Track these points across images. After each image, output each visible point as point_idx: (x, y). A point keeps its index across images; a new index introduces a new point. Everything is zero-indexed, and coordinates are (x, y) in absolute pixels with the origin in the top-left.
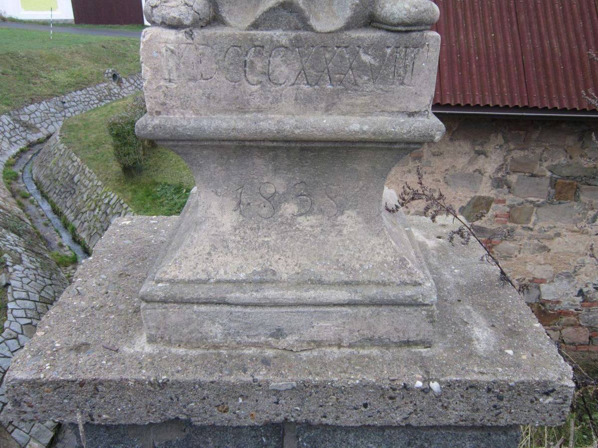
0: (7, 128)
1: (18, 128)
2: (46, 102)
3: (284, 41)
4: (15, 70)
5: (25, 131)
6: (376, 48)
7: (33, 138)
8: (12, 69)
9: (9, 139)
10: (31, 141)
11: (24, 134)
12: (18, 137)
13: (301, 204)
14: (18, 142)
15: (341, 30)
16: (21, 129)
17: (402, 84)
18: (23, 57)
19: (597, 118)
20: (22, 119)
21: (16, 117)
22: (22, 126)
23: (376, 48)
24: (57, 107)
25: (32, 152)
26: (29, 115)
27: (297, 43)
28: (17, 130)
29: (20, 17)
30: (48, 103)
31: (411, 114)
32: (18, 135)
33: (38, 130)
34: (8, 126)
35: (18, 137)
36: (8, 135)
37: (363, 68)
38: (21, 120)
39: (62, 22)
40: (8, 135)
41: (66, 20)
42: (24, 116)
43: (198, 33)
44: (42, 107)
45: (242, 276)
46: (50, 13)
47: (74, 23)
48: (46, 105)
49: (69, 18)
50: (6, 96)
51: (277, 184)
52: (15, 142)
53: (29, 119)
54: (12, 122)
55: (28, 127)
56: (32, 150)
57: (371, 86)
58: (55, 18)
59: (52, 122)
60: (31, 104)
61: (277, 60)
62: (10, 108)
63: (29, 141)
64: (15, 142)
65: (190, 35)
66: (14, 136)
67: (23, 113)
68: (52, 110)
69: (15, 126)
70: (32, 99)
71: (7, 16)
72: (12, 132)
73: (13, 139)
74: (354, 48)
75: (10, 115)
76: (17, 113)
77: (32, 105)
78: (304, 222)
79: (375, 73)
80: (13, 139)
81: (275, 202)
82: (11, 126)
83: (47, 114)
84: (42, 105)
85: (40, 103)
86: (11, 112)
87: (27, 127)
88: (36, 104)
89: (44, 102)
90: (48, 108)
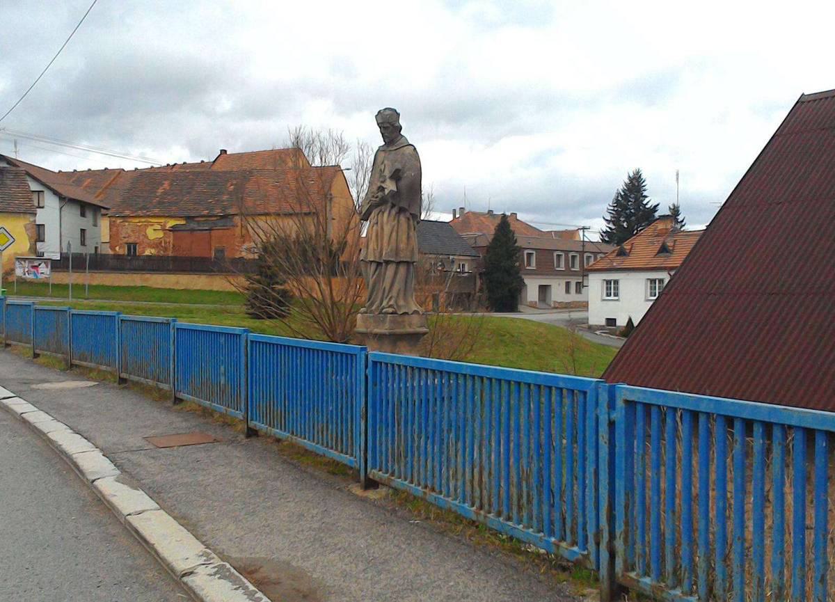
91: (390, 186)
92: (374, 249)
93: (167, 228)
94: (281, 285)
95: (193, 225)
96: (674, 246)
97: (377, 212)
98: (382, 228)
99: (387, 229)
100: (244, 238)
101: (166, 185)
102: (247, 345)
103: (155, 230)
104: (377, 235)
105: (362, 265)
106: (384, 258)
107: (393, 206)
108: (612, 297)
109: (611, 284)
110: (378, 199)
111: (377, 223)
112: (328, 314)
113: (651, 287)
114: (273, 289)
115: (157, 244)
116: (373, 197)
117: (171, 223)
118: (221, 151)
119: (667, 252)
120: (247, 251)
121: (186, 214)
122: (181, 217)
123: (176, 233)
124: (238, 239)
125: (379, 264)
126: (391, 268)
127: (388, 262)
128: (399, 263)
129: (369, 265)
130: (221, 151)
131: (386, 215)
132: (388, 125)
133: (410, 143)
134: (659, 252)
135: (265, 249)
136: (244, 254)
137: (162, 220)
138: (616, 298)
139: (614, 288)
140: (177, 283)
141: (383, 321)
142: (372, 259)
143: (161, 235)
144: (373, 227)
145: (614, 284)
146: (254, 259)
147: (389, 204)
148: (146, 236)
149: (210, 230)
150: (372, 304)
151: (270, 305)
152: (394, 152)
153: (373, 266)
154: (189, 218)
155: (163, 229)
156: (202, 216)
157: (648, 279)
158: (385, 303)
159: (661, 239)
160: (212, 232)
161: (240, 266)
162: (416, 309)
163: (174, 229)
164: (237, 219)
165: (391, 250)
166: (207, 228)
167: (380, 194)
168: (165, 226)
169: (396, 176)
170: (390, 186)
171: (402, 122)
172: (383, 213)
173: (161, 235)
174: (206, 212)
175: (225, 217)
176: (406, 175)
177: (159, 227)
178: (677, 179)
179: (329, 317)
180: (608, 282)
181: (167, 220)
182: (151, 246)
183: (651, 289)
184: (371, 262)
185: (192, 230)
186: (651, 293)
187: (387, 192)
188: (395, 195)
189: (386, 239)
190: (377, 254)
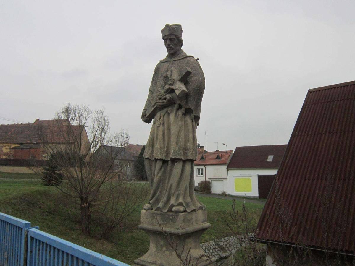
0: (212, 247)
1: (217, 249)
2: (233, 237)
3: (159, 213)
4: (223, 219)
5: (220, 250)
6: (172, 215)
7: (223, 255)
8: (222, 219)
9: (211, 253)
10: (222, 256)
11: (219, 252)
12: (216, 253)
13: (166, 248)
14: (215, 256)
15: (166, 212)
16: (218, 249)
17: (176, 223)
18: (228, 213)
19: (353, 257)
20: (220, 244)
21: (217, 242)
22: (219, 248)
23: (172, 215)
24: (238, 240)
25: (221, 262)
26: (224, 242)
27: (161, 214)
28: (216, 249)
29: (233, 194)
30: (234, 237)
31: (178, 229)
32: (216, 252)
33: (226, 251)
34: (212, 246)
35: (216, 253)
36: (211, 251)
37: (170, 219)
38: (219, 245)
39: (252, 198)
40: (211, 251)
41: (254, 196)
42: (221, 242)
43: (148, 211)
44: (231, 239)
45: (151, 261)
46: (245, 193)
47: (258, 198)
48: (233, 238)
49: (256, 196)
50: (216, 231)
51: (162, 243)
52: (214, 256)
53: (223, 245)
54: (215, 245)
55: (222, 249)
56: (221, 261)
57: (171, 223)
58: (247, 195)
59: (234, 248)
60: (226, 237)
61: (158, 217)
62: (215, 238)
63: (221, 256)
64: (214, 256)
65: (147, 211)
66: (214, 252)
67: (221, 241)
68: (236, 241)
69: (216, 247)
70: (227, 234)
71: (227, 193)
72: (214, 250)
73: (213, 254)
74: (169, 215)
75: (215, 241)
76: (218, 240)
77: (226, 238)
78: (167, 252)
79: (172, 220)
80: (213, 254)
81: (162, 246)
82: (214, 247)
83: (233, 243)
84: (231, 238)
85: (230, 237)
86: (216, 240)
87: (221, 248)
88: (228, 237)
89: (232, 237)
90: (234, 240)
91: (180, 87)
92: (161, 148)
93: (12, 148)
94: (58, 171)
95: (22, 147)
96: (206, 157)
97: (162, 114)
98: (169, 129)
99: (174, 129)
100: (44, 152)
101: (13, 131)
102: (27, 240)
103: (6, 148)
104: (164, 135)
105: (146, 163)
106: (172, 155)
107: (180, 107)
108: (201, 175)
109: (200, 170)
110: (165, 101)
111: (163, 124)
112: (80, 184)
113: (198, 171)
114: (55, 173)
115: (7, 154)
116: (160, 99)
117: (13, 146)
118: (37, 119)
119: (204, 159)
120: (45, 157)
121: (20, 142)
122: (18, 144)
123: (15, 150)
124: (41, 153)
125: (164, 162)
126: (178, 167)
127: (174, 161)
128: (184, 162)
129: (154, 163)
130: (37, 119)
131: (172, 116)
132: (175, 37)
133: (188, 55)
134: (201, 159)
135: (52, 156)
136: (43, 158)
137: (10, 145)
138: (202, 175)
139: (201, 172)
140: (14, 170)
141: (174, 220)
142: (159, 157)
143: (8, 150)
144: (159, 127)
145: (201, 170)
146: (47, 161)
147: (176, 106)
148: (2, 151)
149: (30, 149)
150: (157, 201)
151: (53, 180)
152: (179, 61)
153: (159, 164)
154: (21, 144)
155: (10, 148)
156: (26, 143)
157: (197, 169)
158: (173, 201)
159: (201, 155)
160: (31, 149)
161: (40, 163)
162: (200, 205)
163: (15, 148)
164: (41, 145)
165: (179, 149)
166: (28, 148)
167: (168, 96)
168: (11, 147)
169: (185, 78)
170: (180, 87)
171: (184, 37)
172: (169, 114)
173: (8, 150)
174: (28, 142)
175: (37, 144)
176: (193, 79)
177: (8, 147)
178: (206, 134)
179: (80, 186)
180: (199, 169)
181: (11, 144)
182: (4, 155)
183: (198, 172)
184: (156, 160)
185: (22, 149)
186: (198, 174)
187: (177, 92)
188: (185, 96)
189: (173, 137)
190: (164, 153)
